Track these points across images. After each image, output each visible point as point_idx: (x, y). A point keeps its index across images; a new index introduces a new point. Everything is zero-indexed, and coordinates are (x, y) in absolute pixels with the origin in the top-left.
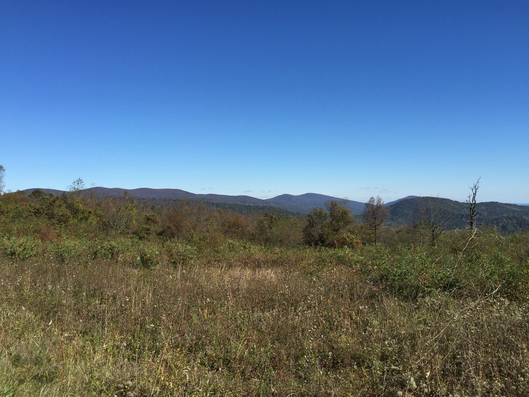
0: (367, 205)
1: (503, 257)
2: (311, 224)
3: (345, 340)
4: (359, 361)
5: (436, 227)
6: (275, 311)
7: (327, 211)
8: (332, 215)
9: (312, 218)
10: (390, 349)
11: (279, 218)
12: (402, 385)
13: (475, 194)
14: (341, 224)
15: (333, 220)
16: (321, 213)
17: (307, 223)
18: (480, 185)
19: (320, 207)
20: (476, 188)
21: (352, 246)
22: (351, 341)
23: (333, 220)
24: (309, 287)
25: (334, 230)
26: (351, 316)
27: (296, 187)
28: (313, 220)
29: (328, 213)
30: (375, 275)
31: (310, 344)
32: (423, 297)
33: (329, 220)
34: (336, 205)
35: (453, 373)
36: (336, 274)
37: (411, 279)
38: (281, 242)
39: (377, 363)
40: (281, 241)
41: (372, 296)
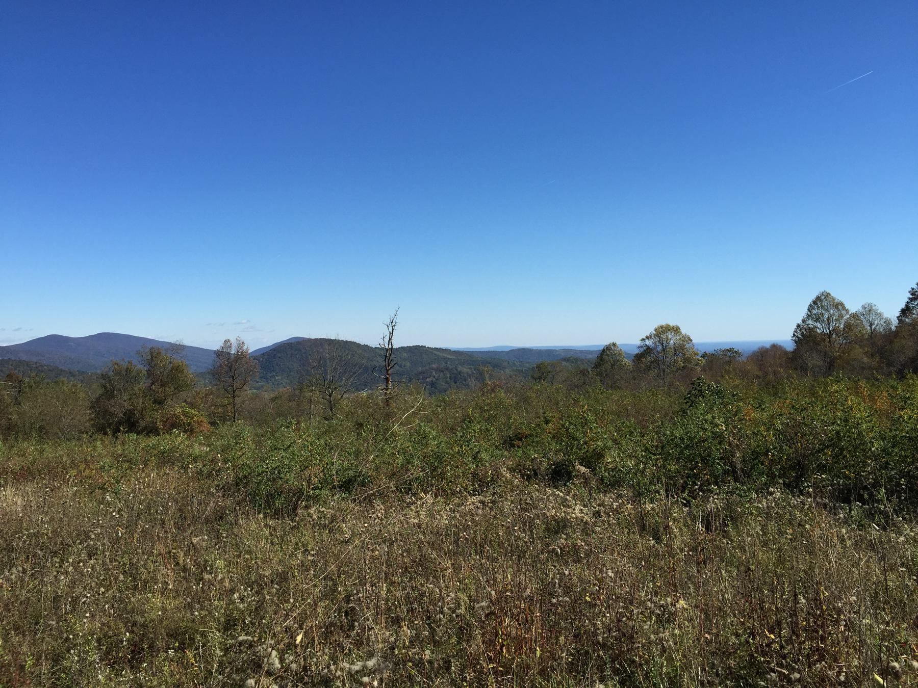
0: (219, 354)
1: (427, 430)
2: (109, 393)
3: (156, 605)
4: (183, 638)
5: (335, 388)
6: (14, 570)
7: (140, 367)
8: (150, 373)
9: (110, 381)
10: (241, 606)
11: (38, 384)
12: (257, 666)
13: (391, 334)
14: (170, 390)
15: (153, 384)
16: (128, 370)
17: (100, 391)
18: (398, 319)
19: (126, 360)
20: (392, 324)
21: (190, 430)
22: (171, 604)
23: (153, 384)
24: (96, 514)
25: (155, 402)
26: (175, 557)
27: (624, 325)
28: (111, 385)
29: (144, 369)
30: (228, 477)
31: (84, 625)
32: (307, 507)
33: (143, 384)
34: (159, 354)
35: (342, 628)
36: (158, 483)
37: (292, 479)
38: (43, 432)
39: (216, 636)
40: (41, 428)
41: (220, 516)
